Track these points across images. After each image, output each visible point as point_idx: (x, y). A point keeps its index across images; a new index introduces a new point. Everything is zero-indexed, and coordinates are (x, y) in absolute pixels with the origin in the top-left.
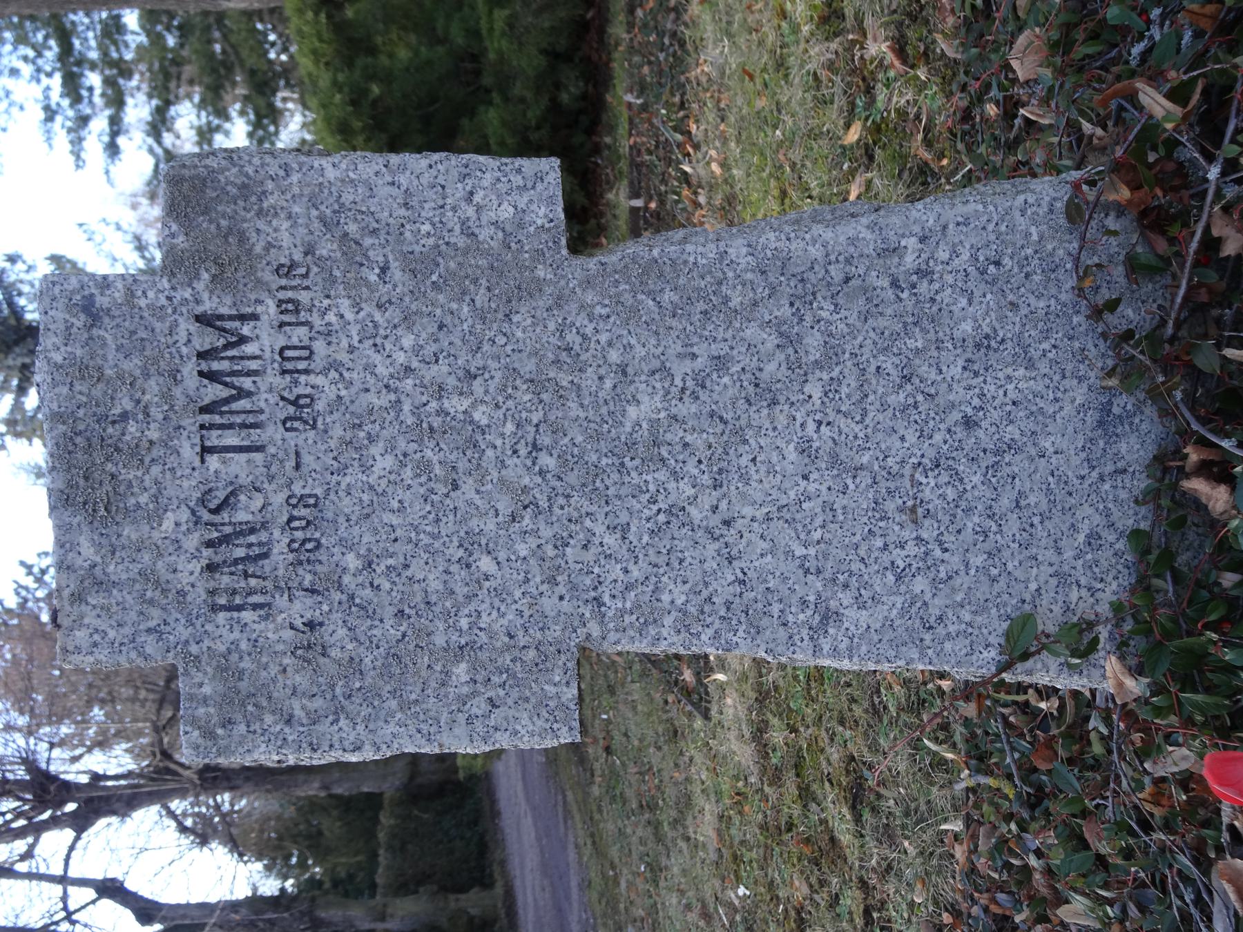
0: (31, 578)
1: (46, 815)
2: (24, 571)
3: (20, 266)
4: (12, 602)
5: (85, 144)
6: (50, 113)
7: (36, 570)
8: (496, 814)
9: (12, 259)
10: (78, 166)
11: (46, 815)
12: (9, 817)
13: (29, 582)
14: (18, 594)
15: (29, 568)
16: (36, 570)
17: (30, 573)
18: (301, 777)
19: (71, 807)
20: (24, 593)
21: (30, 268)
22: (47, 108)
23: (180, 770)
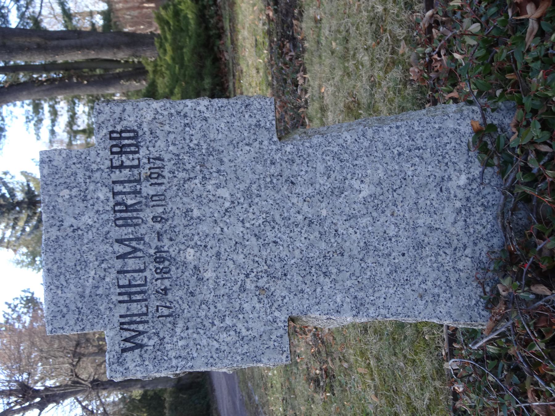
0: (10, 310)
1: (27, 404)
2: (7, 306)
3: (8, 176)
4: (2, 320)
5: (41, 130)
6: (28, 120)
7: (12, 306)
8: (213, 390)
9: (5, 173)
10: (38, 139)
11: (27, 404)
12: (12, 405)
13: (9, 311)
14: (4, 317)
15: (9, 305)
16: (12, 306)
17: (10, 307)
18: (133, 383)
19: (38, 400)
20: (7, 316)
21: (13, 177)
22: (27, 118)
23: (83, 382)
